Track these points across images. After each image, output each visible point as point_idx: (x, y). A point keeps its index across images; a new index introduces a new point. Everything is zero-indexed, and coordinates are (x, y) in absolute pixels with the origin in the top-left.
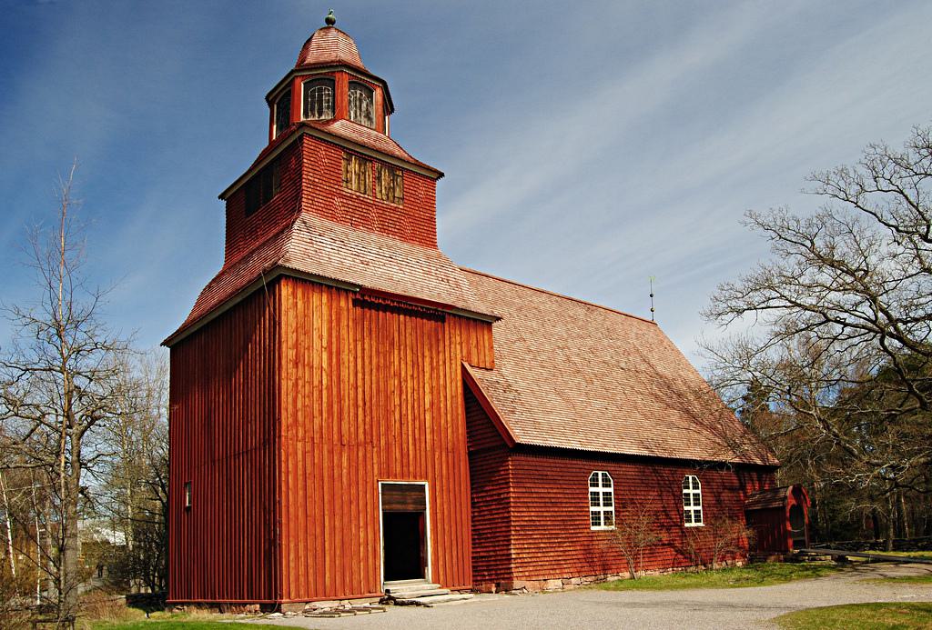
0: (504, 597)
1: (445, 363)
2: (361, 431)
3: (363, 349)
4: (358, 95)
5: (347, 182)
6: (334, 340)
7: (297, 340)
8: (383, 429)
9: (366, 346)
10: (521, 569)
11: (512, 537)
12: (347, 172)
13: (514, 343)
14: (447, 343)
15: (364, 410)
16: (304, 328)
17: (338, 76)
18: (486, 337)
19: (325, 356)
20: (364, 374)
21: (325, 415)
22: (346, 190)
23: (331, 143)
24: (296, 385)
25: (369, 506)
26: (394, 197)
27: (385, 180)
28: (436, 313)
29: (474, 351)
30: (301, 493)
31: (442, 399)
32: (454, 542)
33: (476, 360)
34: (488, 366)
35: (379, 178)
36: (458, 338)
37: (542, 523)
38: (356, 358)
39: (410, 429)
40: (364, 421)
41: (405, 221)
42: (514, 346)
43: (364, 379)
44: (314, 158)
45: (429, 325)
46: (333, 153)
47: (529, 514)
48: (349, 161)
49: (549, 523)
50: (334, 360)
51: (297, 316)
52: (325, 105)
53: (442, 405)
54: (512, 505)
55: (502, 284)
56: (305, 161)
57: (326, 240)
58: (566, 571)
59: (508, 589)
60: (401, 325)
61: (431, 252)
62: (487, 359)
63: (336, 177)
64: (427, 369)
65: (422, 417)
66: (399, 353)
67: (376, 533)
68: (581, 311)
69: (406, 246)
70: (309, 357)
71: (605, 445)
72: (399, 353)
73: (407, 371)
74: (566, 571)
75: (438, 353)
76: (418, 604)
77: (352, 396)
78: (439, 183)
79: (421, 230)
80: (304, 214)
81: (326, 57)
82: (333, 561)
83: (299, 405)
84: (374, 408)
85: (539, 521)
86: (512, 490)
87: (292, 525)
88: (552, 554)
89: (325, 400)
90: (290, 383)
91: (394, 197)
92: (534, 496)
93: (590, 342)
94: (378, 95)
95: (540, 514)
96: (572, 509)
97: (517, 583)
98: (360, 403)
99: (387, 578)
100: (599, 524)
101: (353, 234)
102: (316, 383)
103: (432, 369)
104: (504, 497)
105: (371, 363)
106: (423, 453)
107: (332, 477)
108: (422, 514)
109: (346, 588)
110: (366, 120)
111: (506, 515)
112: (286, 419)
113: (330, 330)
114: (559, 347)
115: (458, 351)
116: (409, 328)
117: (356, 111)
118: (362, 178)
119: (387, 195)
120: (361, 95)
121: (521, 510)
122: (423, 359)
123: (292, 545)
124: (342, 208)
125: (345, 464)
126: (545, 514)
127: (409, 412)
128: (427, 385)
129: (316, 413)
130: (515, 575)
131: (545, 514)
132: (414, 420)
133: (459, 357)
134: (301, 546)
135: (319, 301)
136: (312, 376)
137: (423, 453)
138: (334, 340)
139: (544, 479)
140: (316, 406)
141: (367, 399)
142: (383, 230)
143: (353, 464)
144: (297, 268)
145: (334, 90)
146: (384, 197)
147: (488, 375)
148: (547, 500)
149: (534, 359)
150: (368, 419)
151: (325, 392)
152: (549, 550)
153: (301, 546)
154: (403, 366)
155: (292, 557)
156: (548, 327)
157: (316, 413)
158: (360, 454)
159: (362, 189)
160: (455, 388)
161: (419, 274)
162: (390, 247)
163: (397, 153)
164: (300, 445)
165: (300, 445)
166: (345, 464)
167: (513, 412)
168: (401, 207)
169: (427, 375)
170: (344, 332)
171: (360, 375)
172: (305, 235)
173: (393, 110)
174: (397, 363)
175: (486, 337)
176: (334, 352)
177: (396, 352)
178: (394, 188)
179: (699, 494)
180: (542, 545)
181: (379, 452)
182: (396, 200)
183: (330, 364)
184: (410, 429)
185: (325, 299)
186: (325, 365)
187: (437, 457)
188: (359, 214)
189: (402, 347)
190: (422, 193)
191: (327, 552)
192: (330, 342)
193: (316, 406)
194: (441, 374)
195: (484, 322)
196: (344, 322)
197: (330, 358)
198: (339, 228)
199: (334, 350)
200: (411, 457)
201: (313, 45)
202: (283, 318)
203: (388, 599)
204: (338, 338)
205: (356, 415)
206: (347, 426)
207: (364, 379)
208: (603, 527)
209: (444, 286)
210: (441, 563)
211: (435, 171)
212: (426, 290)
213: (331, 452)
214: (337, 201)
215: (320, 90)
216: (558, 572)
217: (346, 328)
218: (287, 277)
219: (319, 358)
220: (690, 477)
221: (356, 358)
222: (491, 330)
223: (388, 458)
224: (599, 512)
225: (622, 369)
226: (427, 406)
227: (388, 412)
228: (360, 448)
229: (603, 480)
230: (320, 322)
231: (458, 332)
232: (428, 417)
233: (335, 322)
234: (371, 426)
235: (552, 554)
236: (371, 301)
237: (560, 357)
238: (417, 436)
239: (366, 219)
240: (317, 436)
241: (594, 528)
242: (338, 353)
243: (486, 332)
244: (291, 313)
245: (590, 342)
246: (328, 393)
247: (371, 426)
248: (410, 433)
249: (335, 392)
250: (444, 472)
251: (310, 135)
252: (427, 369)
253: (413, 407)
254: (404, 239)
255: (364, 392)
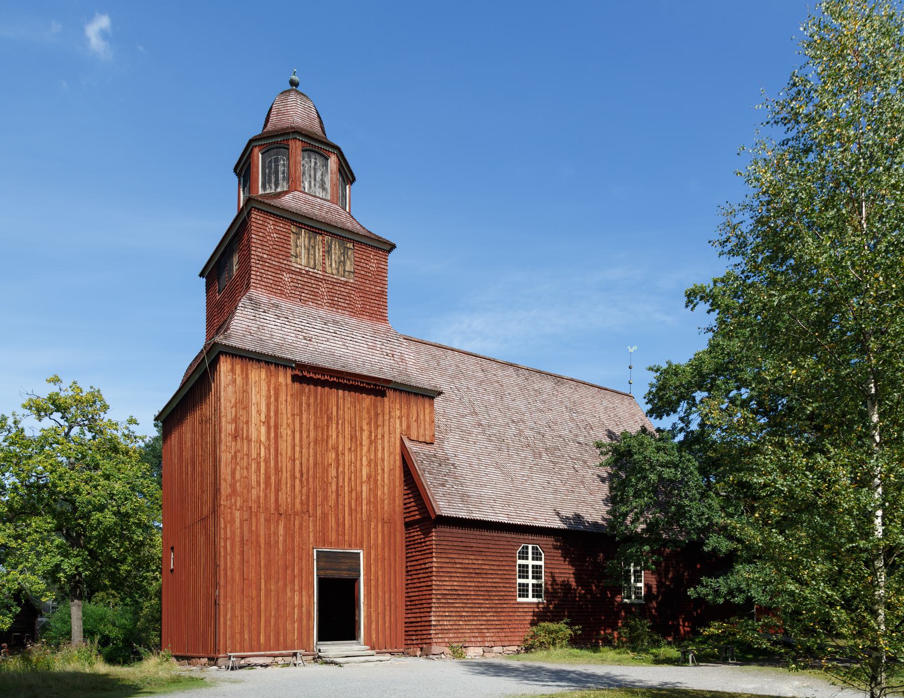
0: (422, 661)
1: (383, 436)
2: (298, 501)
3: (301, 424)
4: (313, 164)
5: (296, 257)
6: (272, 414)
7: (236, 415)
8: (319, 500)
9: (304, 421)
10: (440, 636)
11: (433, 605)
12: (297, 246)
13: (463, 416)
14: (387, 417)
15: (301, 481)
16: (243, 404)
17: (291, 143)
18: (427, 411)
19: (263, 430)
20: (301, 447)
21: (262, 486)
22: (295, 265)
23: (280, 216)
24: (235, 457)
25: (304, 572)
26: (345, 271)
27: (335, 254)
28: (374, 387)
29: (414, 425)
30: (238, 557)
31: (380, 471)
32: (387, 608)
33: (416, 435)
34: (428, 440)
35: (329, 252)
36: (398, 413)
37: (465, 593)
38: (293, 432)
39: (346, 500)
40: (301, 491)
41: (355, 295)
42: (464, 420)
43: (301, 452)
44: (264, 231)
45: (367, 400)
46: (282, 226)
47: (451, 583)
48: (298, 234)
49: (472, 593)
50: (272, 435)
51: (236, 392)
52: (281, 176)
53: (379, 478)
54: (434, 574)
55: (466, 357)
56: (253, 236)
57: (270, 316)
58: (488, 639)
59: (426, 654)
60: (342, 403)
61: (381, 327)
62: (427, 432)
63: (283, 251)
64: (365, 442)
65: (359, 489)
66: (337, 427)
67: (310, 596)
68: (548, 385)
69: (354, 321)
70: (248, 431)
71: (536, 519)
72: (337, 427)
73: (345, 444)
74: (488, 639)
75: (377, 427)
76: (336, 664)
77: (289, 468)
78: (392, 257)
79: (369, 300)
80: (253, 292)
81: (280, 126)
82: (268, 621)
83: (238, 476)
84: (311, 480)
85: (462, 590)
86: (435, 560)
87: (229, 587)
88: (474, 623)
89: (262, 471)
90: (229, 456)
91: (345, 271)
92: (458, 566)
93: (550, 415)
94: (333, 162)
95: (462, 584)
96: (497, 580)
97: (435, 649)
98: (298, 475)
99: (322, 637)
100: (527, 596)
101: (298, 308)
102: (254, 455)
103: (371, 443)
104: (421, 563)
105: (308, 437)
106: (359, 523)
107: (268, 544)
108: (354, 582)
109: (281, 646)
110: (321, 190)
111: (429, 583)
112: (225, 489)
113: (268, 405)
114: (513, 422)
115: (398, 425)
116: (348, 405)
117: (310, 182)
118: (312, 252)
119: (338, 269)
120: (316, 163)
121: (443, 579)
122: (361, 434)
123: (229, 605)
124: (292, 284)
125: (281, 532)
126: (469, 584)
127: (346, 484)
128: (364, 459)
129: (254, 484)
130: (434, 640)
131: (469, 584)
132: (350, 492)
133: (398, 431)
134: (238, 606)
135: (258, 375)
136: (249, 449)
137: (359, 523)
138: (272, 414)
139: (466, 549)
140: (254, 477)
141: (304, 470)
142: (333, 305)
143: (289, 533)
144: (234, 345)
145: (288, 159)
146: (335, 272)
147: (426, 448)
148: (471, 571)
149: (484, 433)
150: (304, 490)
151: (262, 464)
152: (472, 618)
153: (238, 606)
154: (340, 439)
155: (229, 616)
156: (507, 400)
157: (254, 484)
158: (297, 523)
159: (312, 263)
160: (391, 463)
161: (364, 348)
162: (335, 322)
163: (349, 225)
164: (237, 514)
165: (237, 514)
166: (281, 532)
167: (443, 485)
168: (351, 281)
169: (365, 449)
170: (282, 407)
171: (297, 449)
172: (249, 312)
173: (354, 179)
174: (334, 436)
175: (427, 411)
176: (273, 427)
177: (334, 426)
178: (344, 262)
179: (541, 566)
180: (464, 614)
181: (315, 522)
182: (347, 273)
183: (268, 438)
184: (346, 500)
185: (263, 375)
186: (263, 439)
187: (372, 526)
188: (308, 289)
189: (340, 422)
190: (373, 266)
191: (263, 614)
192: (268, 417)
193: (254, 477)
194: (380, 447)
195: (429, 395)
196: (282, 397)
197: (268, 432)
198: (285, 304)
199: (272, 424)
200: (347, 526)
201: (274, 112)
202: (222, 394)
203: (318, 659)
204: (276, 412)
205: (293, 486)
206: (284, 497)
207: (301, 452)
208: (530, 599)
209: (388, 361)
210: (374, 626)
211: (386, 243)
212: (368, 366)
213: (268, 520)
214: (286, 277)
215: (277, 160)
216: (479, 639)
217: (284, 403)
218: (226, 354)
219: (258, 431)
220: (530, 547)
221: (293, 432)
222: (433, 405)
223: (323, 527)
224: (527, 585)
225: (579, 443)
226: (364, 478)
227: (326, 484)
228: (297, 517)
229: (533, 553)
230: (258, 398)
231: (398, 406)
232: (364, 488)
233: (274, 397)
234: (308, 497)
235: (474, 623)
236: (312, 377)
237: (513, 430)
238: (353, 507)
239: (316, 294)
240: (254, 506)
241: (520, 600)
242: (276, 427)
243: (427, 406)
244: (230, 389)
245: (550, 415)
246: (266, 464)
247: (308, 497)
248: (346, 503)
249: (272, 464)
250: (380, 541)
251: (259, 209)
252: (365, 442)
253: (350, 479)
254: (354, 313)
255: (301, 464)
